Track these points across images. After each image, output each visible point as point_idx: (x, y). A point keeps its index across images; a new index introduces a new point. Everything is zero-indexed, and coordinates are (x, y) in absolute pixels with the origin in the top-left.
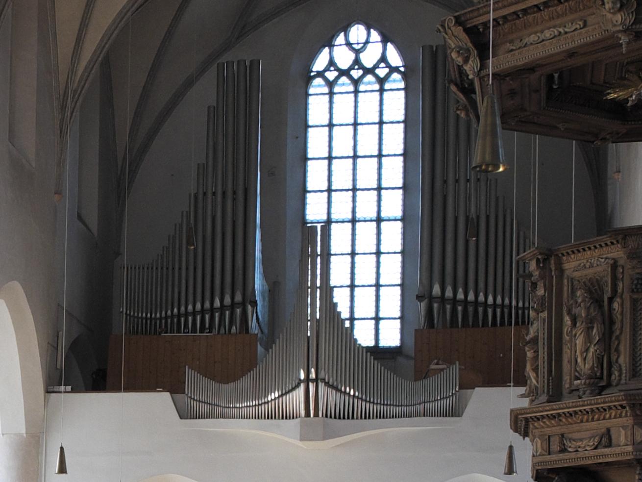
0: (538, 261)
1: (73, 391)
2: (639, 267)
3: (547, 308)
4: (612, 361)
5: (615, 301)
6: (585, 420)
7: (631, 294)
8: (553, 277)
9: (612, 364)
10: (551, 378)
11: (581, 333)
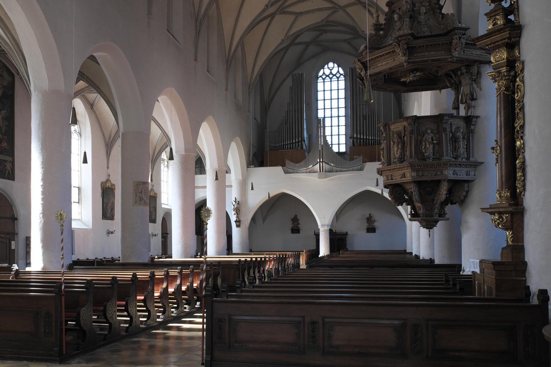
0: (383, 126)
1: (255, 167)
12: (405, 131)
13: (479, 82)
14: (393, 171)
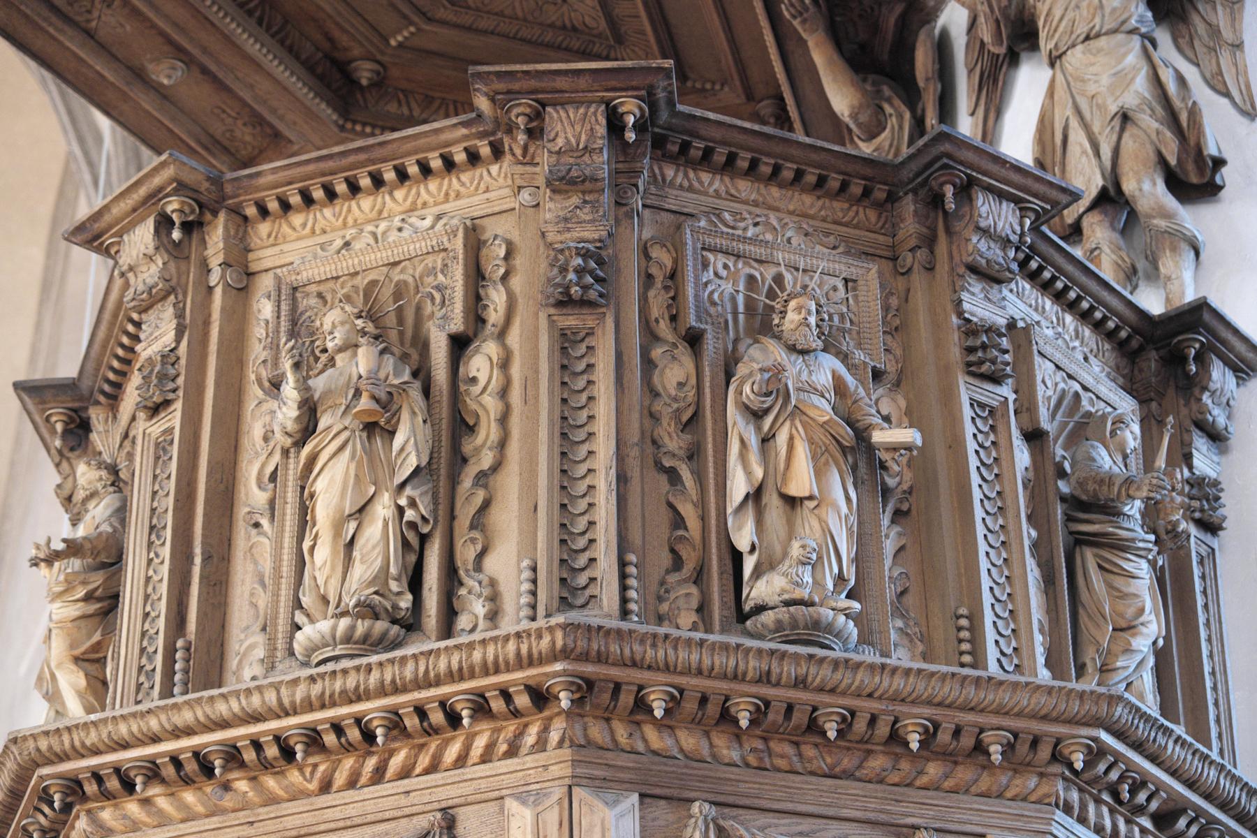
0: (164, 223)
2: (587, 218)
3: (181, 393)
4: (459, 563)
5: (477, 351)
6: (340, 778)
7: (552, 311)
8: (210, 289)
9: (461, 572)
10: (180, 643)
11: (341, 448)
12: (477, 276)
13: (1227, 34)
14: (270, 782)
